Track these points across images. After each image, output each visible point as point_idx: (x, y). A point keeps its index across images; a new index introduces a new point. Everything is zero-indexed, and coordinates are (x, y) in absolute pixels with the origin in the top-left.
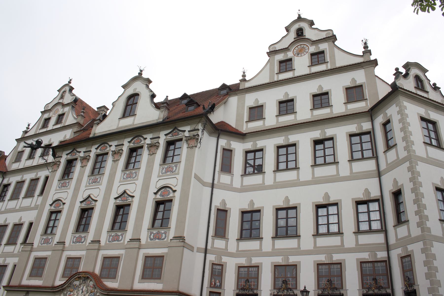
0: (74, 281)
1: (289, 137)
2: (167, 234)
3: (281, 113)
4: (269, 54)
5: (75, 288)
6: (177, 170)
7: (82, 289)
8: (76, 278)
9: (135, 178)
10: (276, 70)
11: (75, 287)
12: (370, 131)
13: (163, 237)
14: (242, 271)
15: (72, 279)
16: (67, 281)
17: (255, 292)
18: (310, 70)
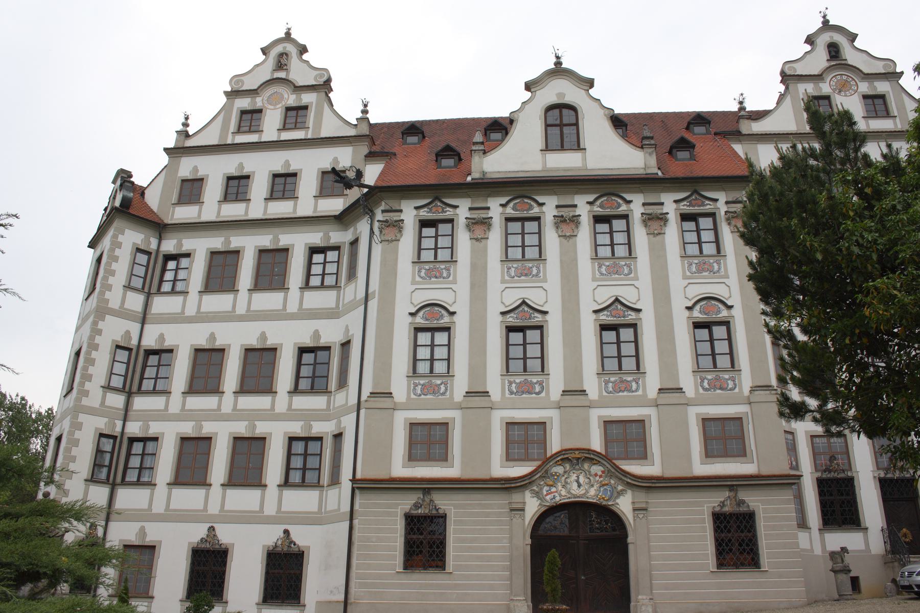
1: (280, 236)
2: (736, 380)
3: (272, 196)
4: (786, 78)
6: (722, 269)
7: (577, 481)
9: (630, 276)
10: (233, 126)
11: (556, 477)
13: (730, 386)
14: (819, 443)
16: (539, 467)
17: (849, 474)
18: (279, 136)
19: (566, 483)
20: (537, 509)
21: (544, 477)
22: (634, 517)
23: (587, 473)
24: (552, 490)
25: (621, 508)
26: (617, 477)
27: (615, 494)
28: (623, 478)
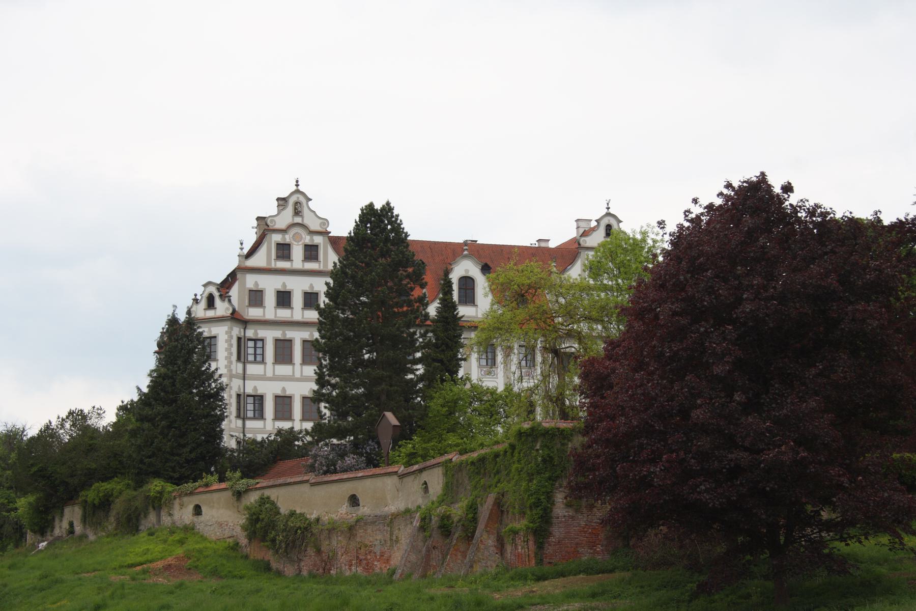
18: (303, 266)
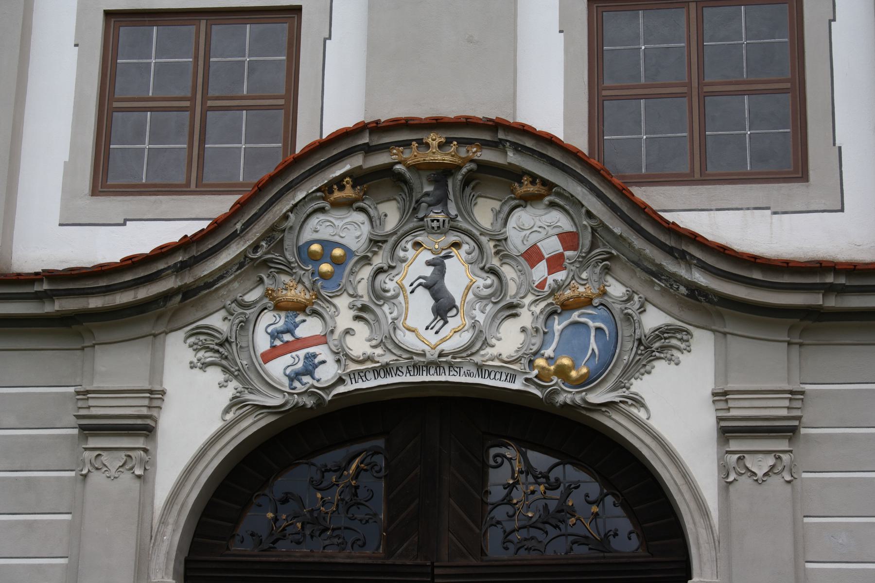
0: (322, 210)
5: (324, 276)
8: (339, 183)
12: (190, 187)
15: (291, 187)
19: (379, 295)
20: (218, 425)
21: (265, 264)
22: (724, 469)
23: (490, 246)
24: (302, 332)
25: (655, 423)
26: (639, 263)
27: (627, 353)
28: (671, 266)
